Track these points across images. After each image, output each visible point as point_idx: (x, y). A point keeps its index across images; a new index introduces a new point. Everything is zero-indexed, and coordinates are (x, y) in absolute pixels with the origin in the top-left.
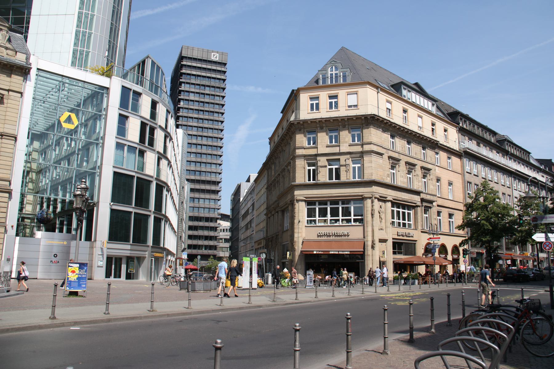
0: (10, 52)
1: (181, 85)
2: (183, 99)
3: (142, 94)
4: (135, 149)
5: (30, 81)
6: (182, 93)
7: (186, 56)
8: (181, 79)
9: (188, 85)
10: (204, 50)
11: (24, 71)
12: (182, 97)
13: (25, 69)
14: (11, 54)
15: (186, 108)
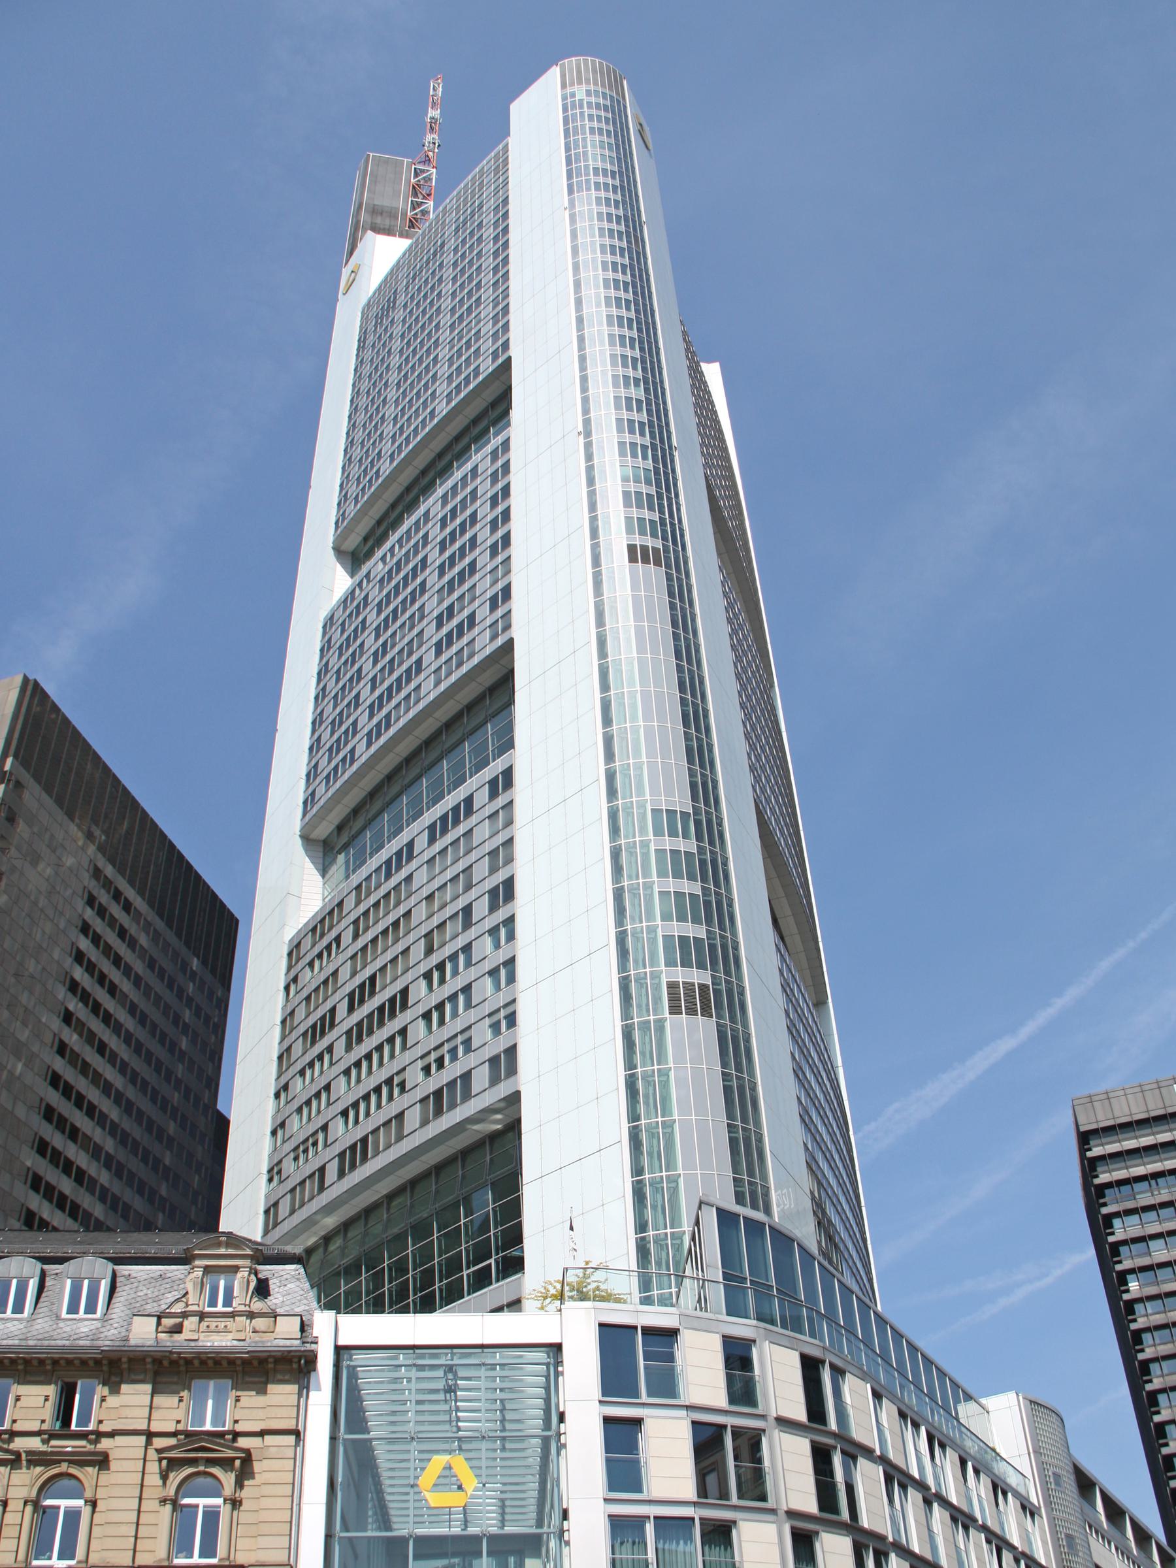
0: (260, 1323)
1: (1111, 1226)
2: (1132, 1271)
3: (679, 1330)
4: (690, 1522)
5: (319, 1389)
6: (1124, 1250)
7: (1094, 1126)
8: (1105, 1205)
9: (1134, 1219)
10: (1161, 1084)
11: (295, 1366)
12: (1127, 1264)
13: (296, 1360)
14: (263, 1329)
15: (1151, 1298)
